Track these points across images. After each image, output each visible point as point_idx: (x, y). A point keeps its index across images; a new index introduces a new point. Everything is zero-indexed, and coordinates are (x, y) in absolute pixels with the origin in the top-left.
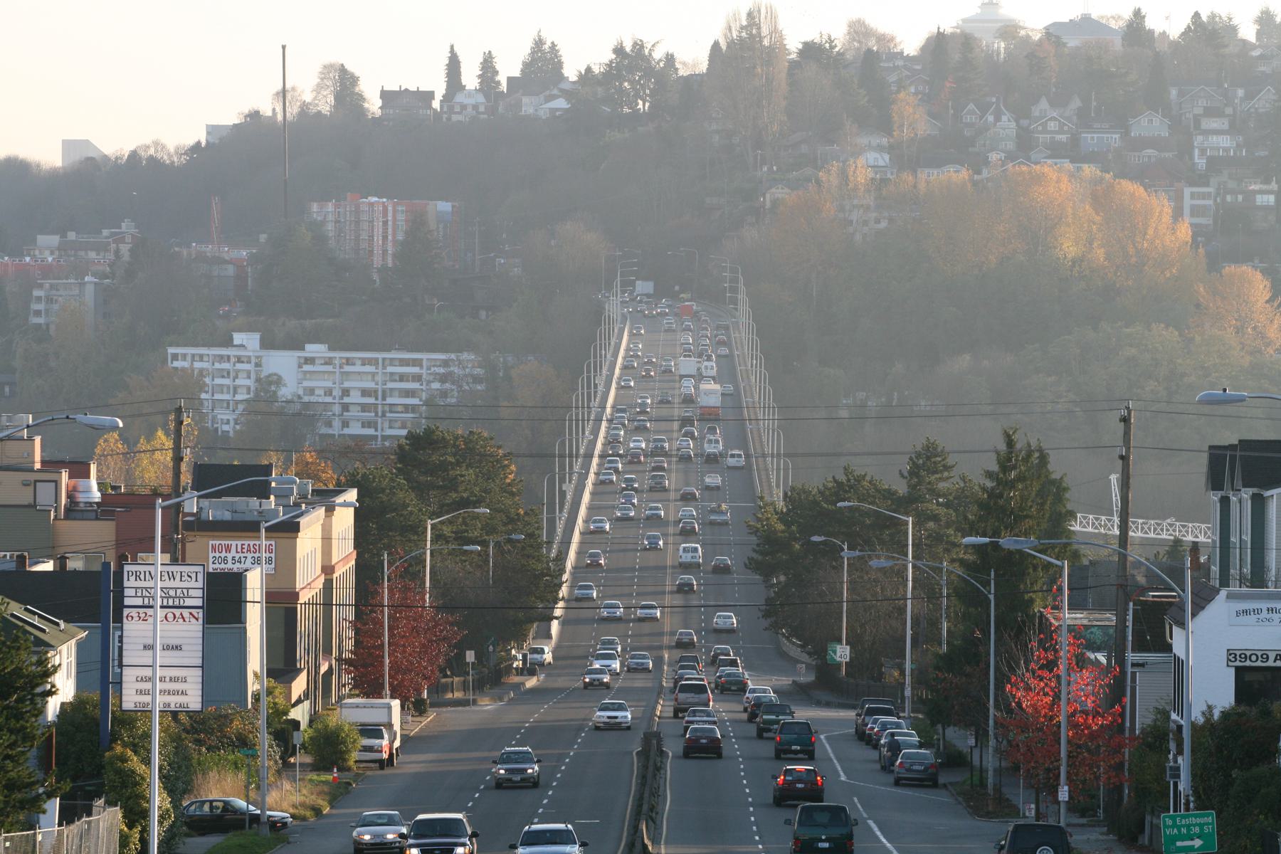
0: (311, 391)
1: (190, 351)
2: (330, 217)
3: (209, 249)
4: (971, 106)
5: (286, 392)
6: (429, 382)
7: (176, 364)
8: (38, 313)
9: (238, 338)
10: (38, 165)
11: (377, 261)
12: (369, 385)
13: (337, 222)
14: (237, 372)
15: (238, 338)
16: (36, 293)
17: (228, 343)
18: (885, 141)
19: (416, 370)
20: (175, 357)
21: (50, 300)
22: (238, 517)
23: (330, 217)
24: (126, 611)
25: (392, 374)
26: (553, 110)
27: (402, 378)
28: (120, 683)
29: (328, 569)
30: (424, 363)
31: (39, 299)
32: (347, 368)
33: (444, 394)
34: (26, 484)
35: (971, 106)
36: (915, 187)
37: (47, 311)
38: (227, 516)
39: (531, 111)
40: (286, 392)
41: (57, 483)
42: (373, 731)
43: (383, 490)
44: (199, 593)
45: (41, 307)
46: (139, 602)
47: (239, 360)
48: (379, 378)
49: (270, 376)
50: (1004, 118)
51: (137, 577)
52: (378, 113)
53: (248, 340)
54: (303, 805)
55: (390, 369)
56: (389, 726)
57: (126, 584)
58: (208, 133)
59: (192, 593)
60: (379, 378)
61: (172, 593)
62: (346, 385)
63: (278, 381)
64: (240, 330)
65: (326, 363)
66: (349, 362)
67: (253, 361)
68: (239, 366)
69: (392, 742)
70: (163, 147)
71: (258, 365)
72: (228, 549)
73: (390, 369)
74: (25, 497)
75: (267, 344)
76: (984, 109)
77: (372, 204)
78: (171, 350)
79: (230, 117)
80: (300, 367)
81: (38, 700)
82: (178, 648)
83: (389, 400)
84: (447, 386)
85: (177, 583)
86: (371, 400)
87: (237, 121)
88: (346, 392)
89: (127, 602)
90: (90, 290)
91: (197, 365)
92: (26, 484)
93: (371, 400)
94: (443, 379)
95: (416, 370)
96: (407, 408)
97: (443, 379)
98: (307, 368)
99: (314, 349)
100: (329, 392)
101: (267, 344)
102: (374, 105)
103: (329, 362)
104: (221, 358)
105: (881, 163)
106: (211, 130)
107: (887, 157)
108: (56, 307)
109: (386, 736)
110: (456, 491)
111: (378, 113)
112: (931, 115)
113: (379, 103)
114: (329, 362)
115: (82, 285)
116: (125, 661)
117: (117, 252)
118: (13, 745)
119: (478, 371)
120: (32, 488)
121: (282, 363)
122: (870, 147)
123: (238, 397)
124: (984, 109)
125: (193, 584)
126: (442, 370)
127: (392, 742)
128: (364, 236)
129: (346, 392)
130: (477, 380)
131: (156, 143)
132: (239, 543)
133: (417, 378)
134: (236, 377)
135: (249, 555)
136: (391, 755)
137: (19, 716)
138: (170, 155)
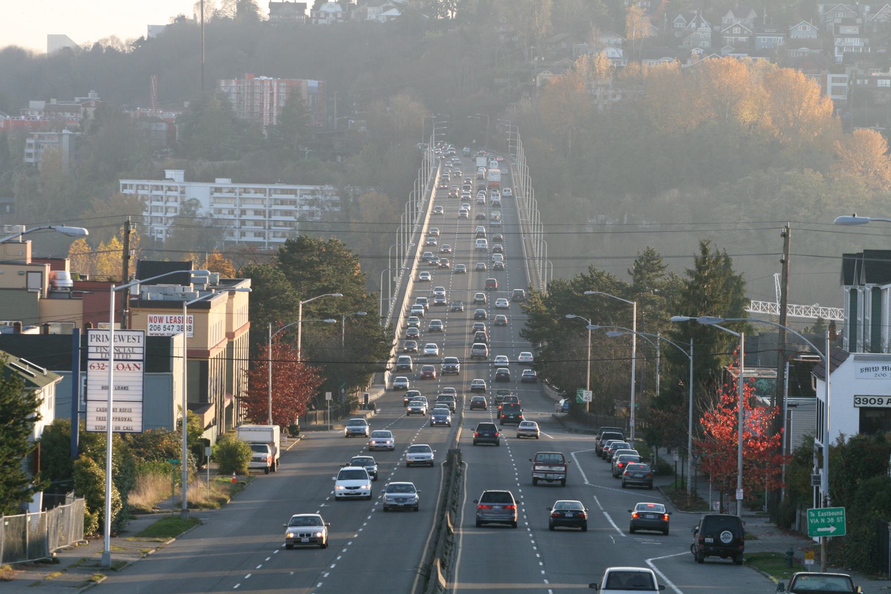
0: (219, 211)
1: (135, 182)
2: (234, 90)
3: (149, 112)
4: (680, 17)
5: (202, 212)
6: (301, 205)
7: (126, 191)
8: (30, 155)
9: (169, 174)
10: (31, 52)
11: (266, 121)
12: (261, 207)
13: (238, 93)
14: (168, 197)
15: (169, 174)
16: (29, 141)
17: (162, 177)
18: (619, 40)
19: (292, 197)
20: (125, 186)
21: (38, 146)
22: (168, 298)
23: (234, 90)
24: (90, 363)
25: (276, 200)
26: (389, 17)
27: (283, 202)
28: (85, 412)
29: (230, 335)
30: (298, 192)
31: (30, 145)
32: (244, 195)
33: (312, 214)
34: (21, 274)
35: (680, 17)
36: (640, 71)
37: (36, 153)
38: (160, 297)
39: (374, 17)
40: (202, 212)
41: (42, 273)
42: (260, 447)
43: (269, 280)
44: (141, 350)
45: (32, 151)
46: (99, 356)
47: (170, 189)
48: (267, 202)
49: (191, 200)
50: (703, 25)
51: (98, 339)
52: (267, 18)
53: (175, 175)
54: (212, 498)
55: (274, 196)
56: (272, 444)
57: (90, 344)
58: (149, 31)
59: (136, 350)
60: (267, 202)
61: (122, 350)
62: (244, 207)
63: (196, 203)
64: (170, 168)
65: (230, 192)
66: (246, 191)
67: (179, 189)
68: (169, 193)
69: (274, 455)
70: (118, 40)
71: (183, 192)
72: (161, 320)
73: (274, 196)
74: (20, 283)
75: (189, 178)
76: (689, 18)
77: (262, 81)
78: (122, 182)
79: (164, 20)
80: (212, 194)
81: (28, 424)
82: (125, 388)
83: (274, 218)
84: (314, 208)
85: (125, 344)
86: (261, 218)
87: (169, 23)
88: (243, 212)
89: (90, 356)
90: (66, 140)
91: (141, 192)
92: (21, 274)
93: (261, 218)
94: (311, 203)
95: (292, 197)
96: (286, 223)
97: (311, 203)
98: (216, 195)
99: (221, 182)
100: (232, 212)
101: (189, 178)
102: (264, 12)
103: (232, 191)
104: (157, 188)
105: (617, 56)
106: (151, 29)
107: (621, 51)
108: (42, 151)
109: (270, 451)
110: (320, 281)
111: (267, 18)
112: (654, 23)
113: (268, 11)
114: (232, 191)
115: (61, 136)
116: (89, 397)
117: (85, 113)
118: (9, 456)
119: (336, 198)
120: (24, 276)
121: (199, 191)
122: (610, 45)
123: (169, 215)
124: (689, 18)
125: (136, 344)
126: (310, 197)
127: (274, 455)
128: (257, 103)
129: (243, 212)
130: (335, 204)
131: (113, 38)
132: (169, 316)
133: (293, 203)
134: (167, 201)
135: (176, 325)
136: (273, 464)
137: (16, 435)
138: (122, 46)
